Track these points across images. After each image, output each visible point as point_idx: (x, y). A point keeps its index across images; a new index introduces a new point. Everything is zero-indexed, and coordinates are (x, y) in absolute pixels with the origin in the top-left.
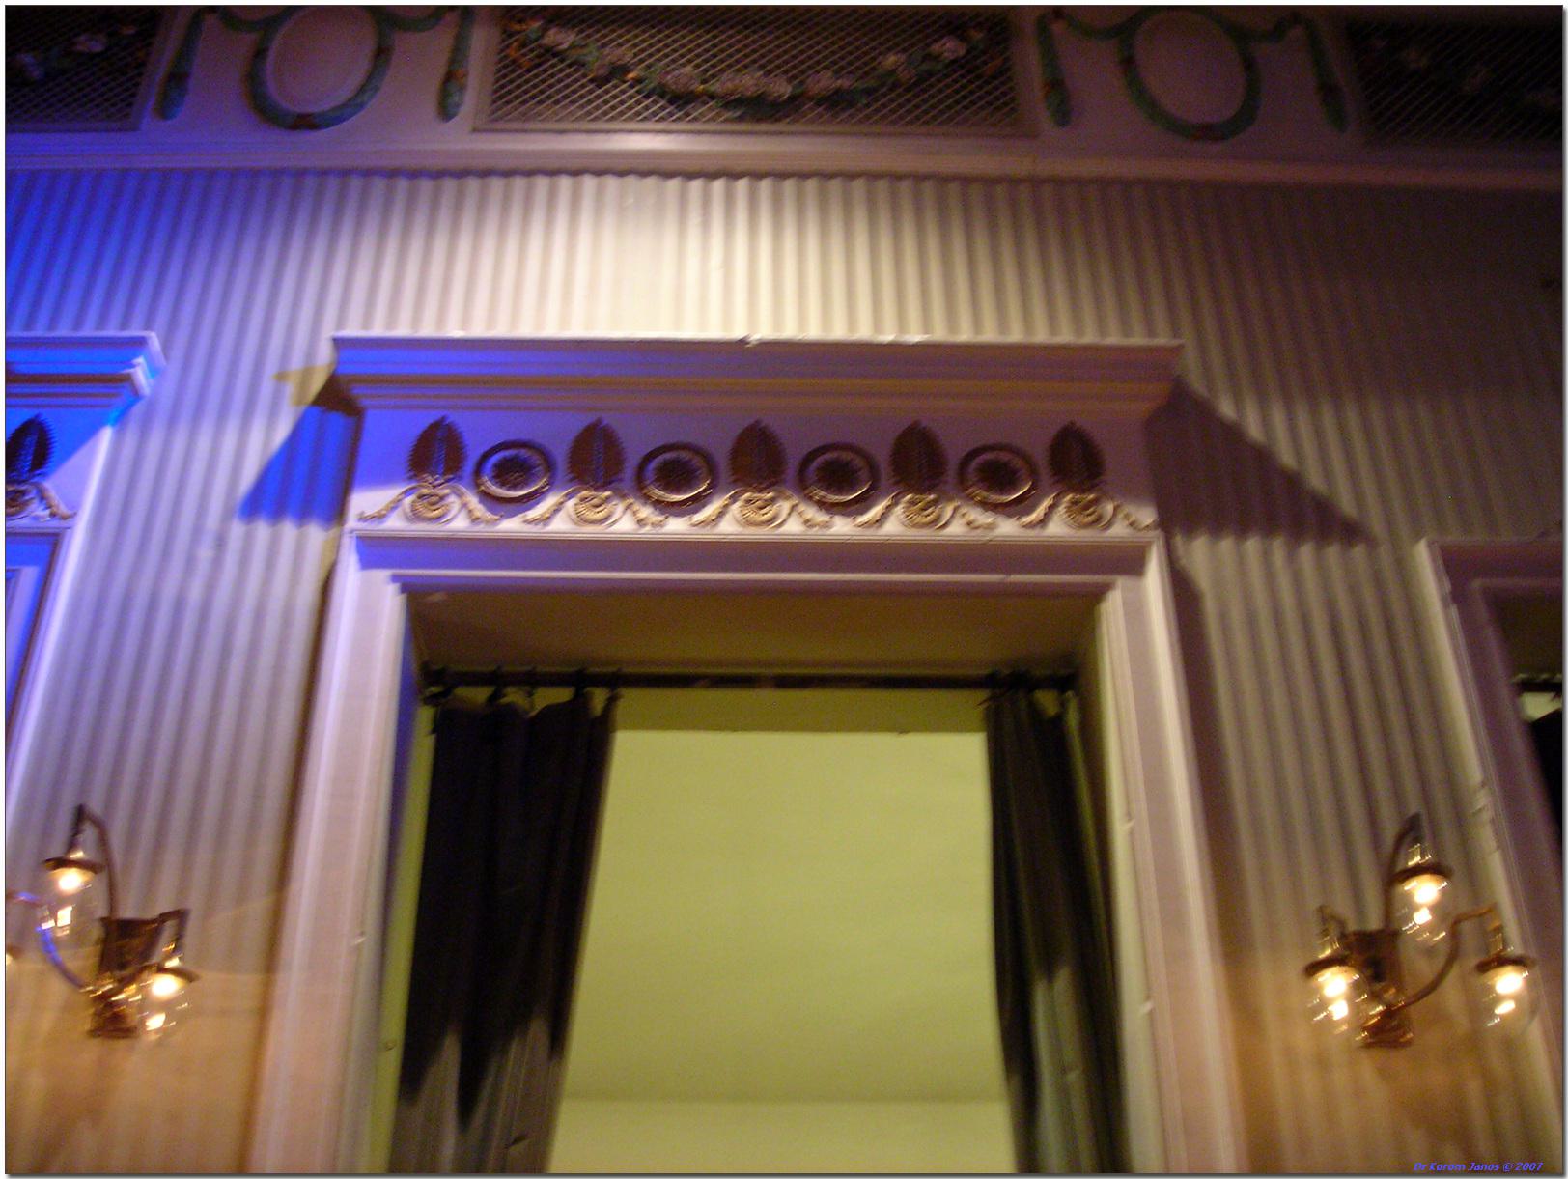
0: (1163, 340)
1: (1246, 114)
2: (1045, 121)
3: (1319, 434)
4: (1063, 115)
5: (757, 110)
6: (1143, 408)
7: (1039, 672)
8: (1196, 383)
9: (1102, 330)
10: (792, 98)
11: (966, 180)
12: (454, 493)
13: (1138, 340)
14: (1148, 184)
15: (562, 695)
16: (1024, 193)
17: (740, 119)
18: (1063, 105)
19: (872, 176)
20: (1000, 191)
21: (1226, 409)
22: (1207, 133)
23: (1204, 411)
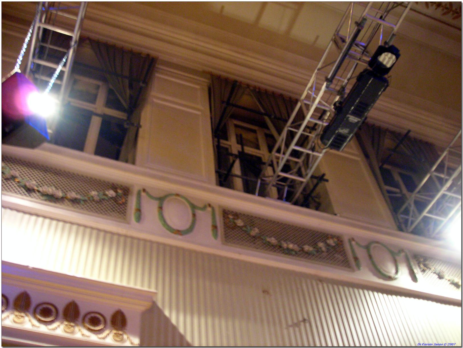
0: (153, 290)
1: (190, 229)
2: (133, 219)
3: (198, 286)
4: (139, 218)
5: (51, 198)
6: (143, 309)
7: (216, 143)
8: (160, 305)
9: (135, 283)
10: (62, 198)
11: (106, 232)
12: (334, 89)
13: (146, 288)
14: (158, 244)
15: (262, 111)
16: (122, 239)
17: (46, 200)
18: (139, 218)
19: (79, 225)
20: (115, 237)
21: (167, 313)
22: (179, 232)
23: (160, 312)
